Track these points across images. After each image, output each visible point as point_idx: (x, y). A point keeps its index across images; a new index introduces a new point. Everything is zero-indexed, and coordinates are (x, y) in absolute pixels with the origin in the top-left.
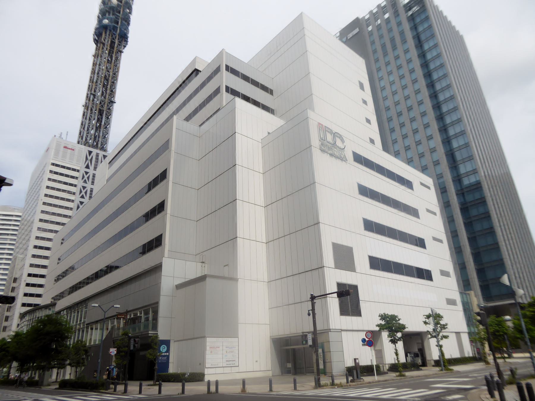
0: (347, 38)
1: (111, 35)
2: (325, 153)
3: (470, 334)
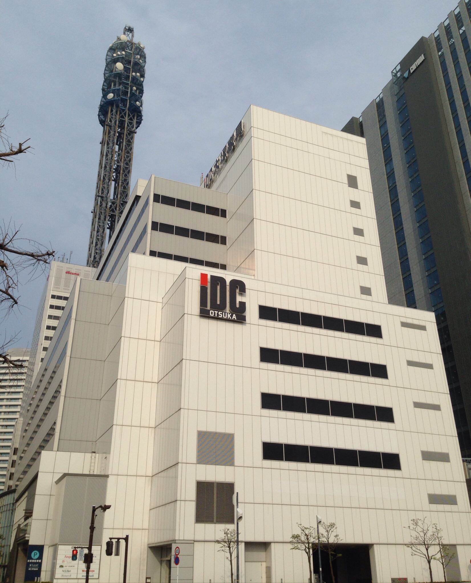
0: (410, 71)
1: (118, 113)
3: (320, 550)
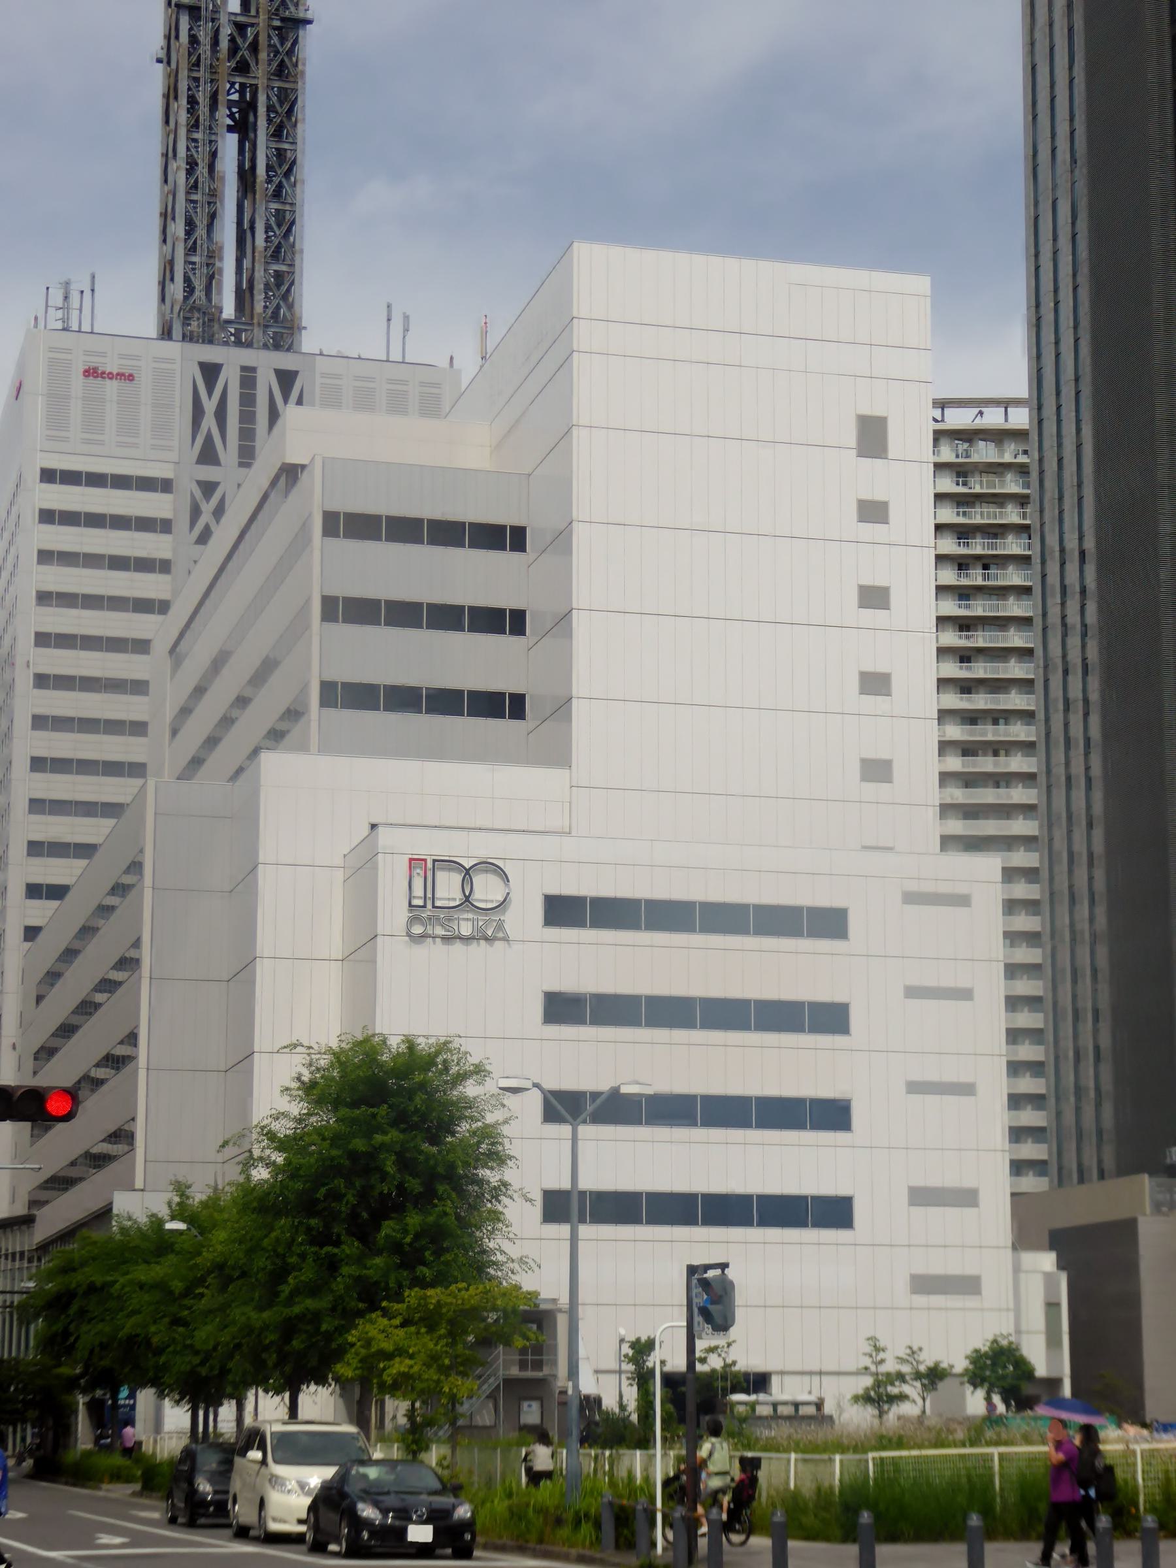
2: (424, 942)
